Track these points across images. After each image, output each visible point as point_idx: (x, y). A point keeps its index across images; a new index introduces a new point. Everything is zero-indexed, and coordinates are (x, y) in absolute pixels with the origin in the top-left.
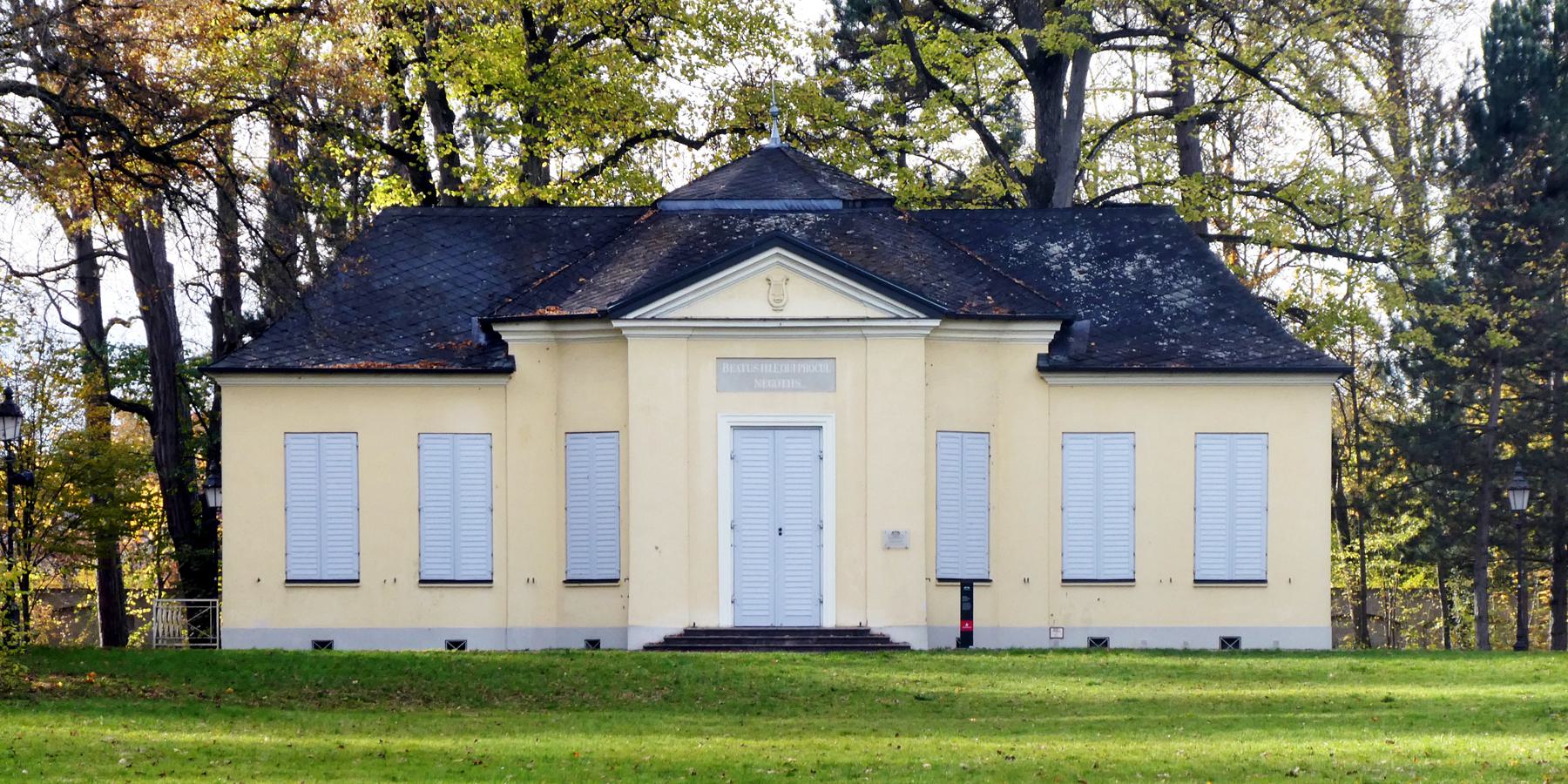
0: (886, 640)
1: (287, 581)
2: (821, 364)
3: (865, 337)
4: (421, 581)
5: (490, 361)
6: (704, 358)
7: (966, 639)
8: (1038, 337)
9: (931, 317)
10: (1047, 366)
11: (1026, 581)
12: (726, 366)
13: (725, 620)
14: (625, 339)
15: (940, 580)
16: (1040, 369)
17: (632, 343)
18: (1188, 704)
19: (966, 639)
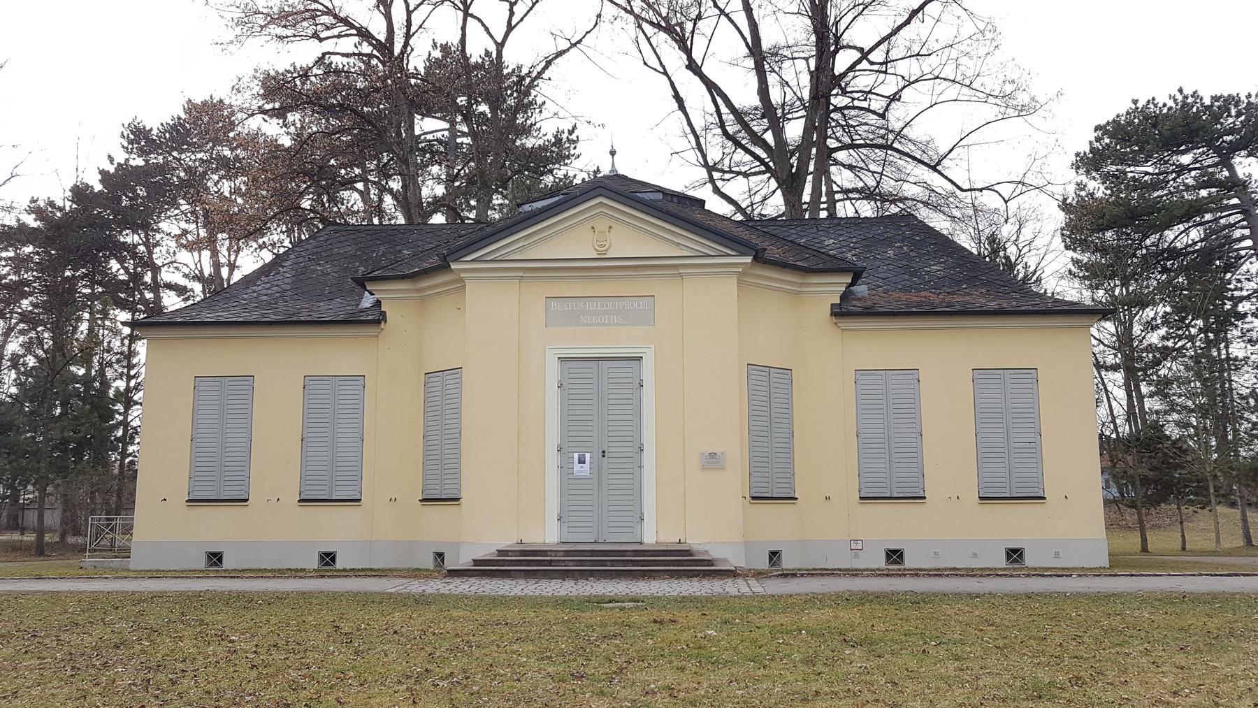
0: (760, 258)
1: (300, 501)
2: (641, 301)
3: (681, 276)
4: (300, 501)
5: (377, 318)
6: (535, 297)
7: (1184, 548)
8: (831, 288)
9: (743, 254)
10: (840, 312)
11: (828, 498)
12: (555, 305)
13: (547, 534)
14: (462, 280)
15: (754, 498)
16: (834, 314)
17: (470, 286)
18: (777, 598)
19: (1184, 548)
